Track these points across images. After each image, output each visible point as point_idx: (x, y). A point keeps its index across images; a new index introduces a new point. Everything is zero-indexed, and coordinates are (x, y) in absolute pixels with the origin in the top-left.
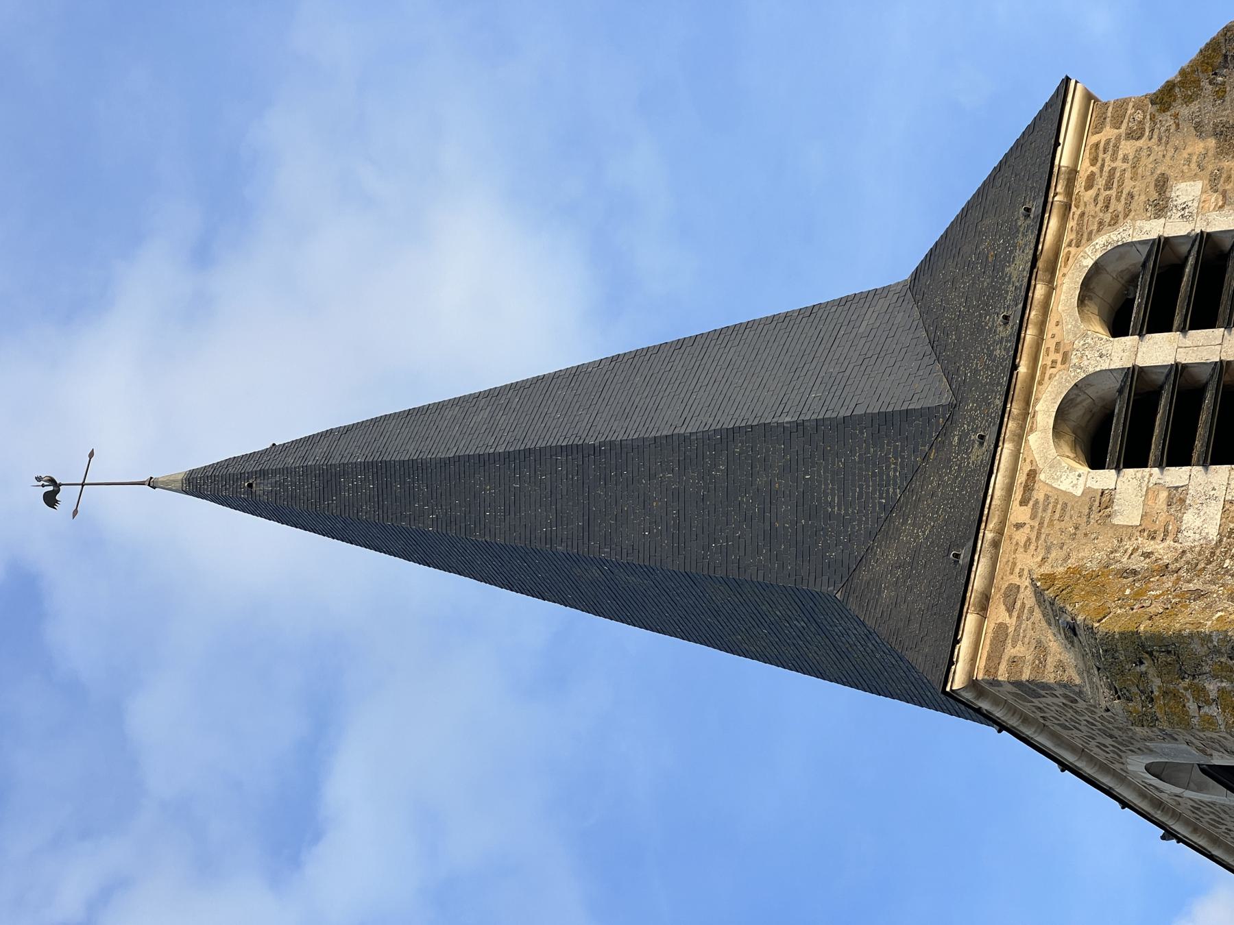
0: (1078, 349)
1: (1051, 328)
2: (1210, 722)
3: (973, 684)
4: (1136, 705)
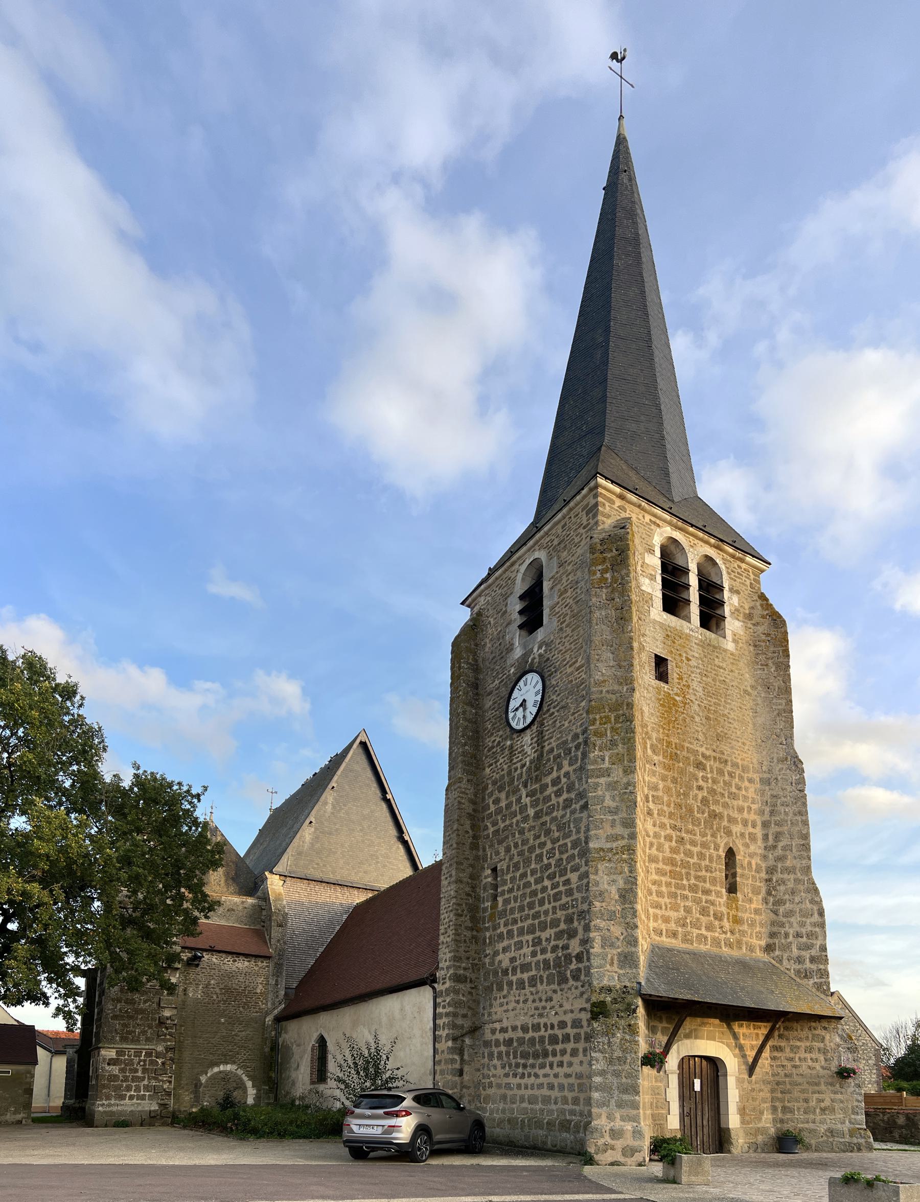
0: (694, 552)
1: (701, 543)
2: (595, 574)
3: (597, 486)
4: (599, 547)
